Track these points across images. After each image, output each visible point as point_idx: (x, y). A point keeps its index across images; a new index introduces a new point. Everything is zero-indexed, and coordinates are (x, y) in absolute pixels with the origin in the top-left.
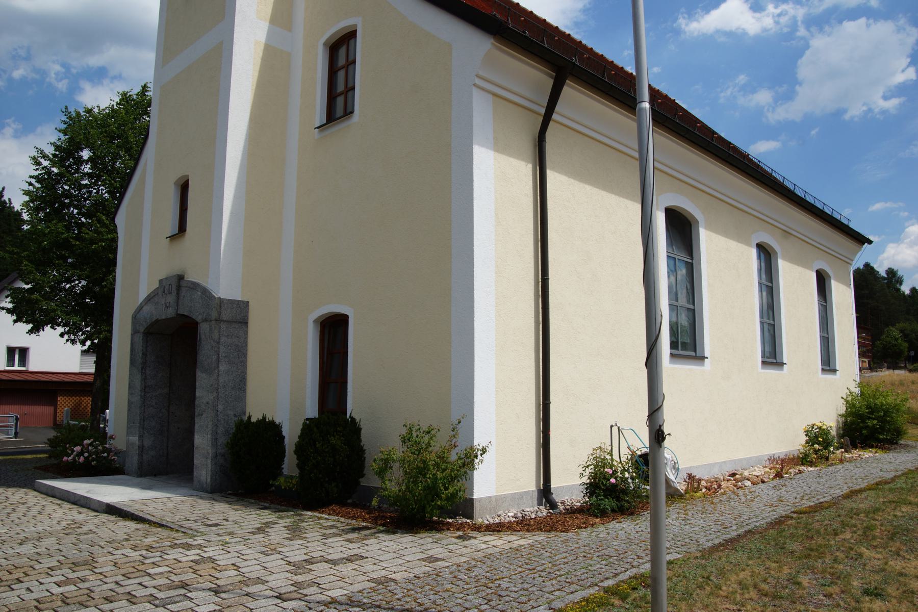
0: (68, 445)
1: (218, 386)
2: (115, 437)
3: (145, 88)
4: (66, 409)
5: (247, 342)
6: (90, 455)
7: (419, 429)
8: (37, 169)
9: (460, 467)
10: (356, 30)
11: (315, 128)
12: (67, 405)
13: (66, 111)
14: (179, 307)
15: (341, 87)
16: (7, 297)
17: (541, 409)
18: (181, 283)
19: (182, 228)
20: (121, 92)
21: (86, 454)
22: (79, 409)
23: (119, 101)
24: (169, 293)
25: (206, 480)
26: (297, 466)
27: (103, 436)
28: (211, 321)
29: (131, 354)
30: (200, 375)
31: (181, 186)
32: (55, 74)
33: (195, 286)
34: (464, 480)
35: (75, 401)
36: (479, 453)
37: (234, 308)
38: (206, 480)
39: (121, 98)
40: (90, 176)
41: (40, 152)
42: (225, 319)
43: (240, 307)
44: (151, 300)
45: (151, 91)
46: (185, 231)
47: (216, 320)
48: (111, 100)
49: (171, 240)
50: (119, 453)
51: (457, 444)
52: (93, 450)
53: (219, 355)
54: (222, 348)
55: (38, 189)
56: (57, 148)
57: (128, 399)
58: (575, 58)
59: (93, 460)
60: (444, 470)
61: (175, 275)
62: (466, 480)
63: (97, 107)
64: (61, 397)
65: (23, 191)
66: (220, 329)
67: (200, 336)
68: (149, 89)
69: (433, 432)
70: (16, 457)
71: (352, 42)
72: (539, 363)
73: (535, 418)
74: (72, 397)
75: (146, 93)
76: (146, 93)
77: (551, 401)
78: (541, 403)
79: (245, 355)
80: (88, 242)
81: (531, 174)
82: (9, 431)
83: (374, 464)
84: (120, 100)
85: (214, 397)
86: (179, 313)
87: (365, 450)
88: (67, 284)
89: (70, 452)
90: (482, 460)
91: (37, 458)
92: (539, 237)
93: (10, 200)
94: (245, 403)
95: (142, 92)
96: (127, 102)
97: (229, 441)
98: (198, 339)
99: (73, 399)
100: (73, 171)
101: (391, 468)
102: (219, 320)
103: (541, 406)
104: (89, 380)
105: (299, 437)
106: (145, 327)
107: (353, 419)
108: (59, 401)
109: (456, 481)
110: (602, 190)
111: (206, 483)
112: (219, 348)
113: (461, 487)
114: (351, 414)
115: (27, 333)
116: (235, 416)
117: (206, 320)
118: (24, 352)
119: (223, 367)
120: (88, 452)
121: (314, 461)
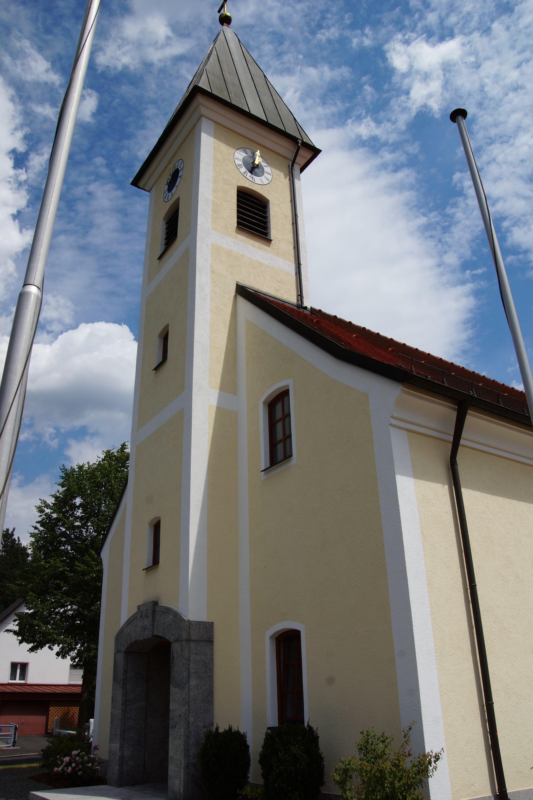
0: (58, 756)
1: (189, 699)
2: (99, 747)
3: (123, 446)
4: (56, 718)
5: (213, 658)
6: (77, 766)
7: (374, 736)
8: (41, 516)
9: (416, 774)
10: (289, 389)
11: (261, 471)
12: (57, 714)
13: (64, 470)
14: (154, 629)
15: (280, 436)
16: (15, 621)
17: (485, 710)
18: (155, 608)
19: (156, 560)
20: (105, 450)
21: (74, 765)
22: (67, 718)
23: (104, 458)
24: (146, 618)
25: (180, 790)
26: (262, 776)
27: (87, 747)
28: (182, 641)
29: (114, 671)
30: (173, 690)
31: (154, 525)
32: (49, 435)
33: (168, 611)
34: (420, 787)
35: (64, 711)
36: (433, 760)
37: (201, 628)
38: (180, 790)
39: (105, 455)
40: (81, 519)
41: (43, 502)
42: (194, 639)
43: (206, 628)
44: (131, 623)
45: (128, 448)
46: (158, 563)
47: (186, 640)
48: (98, 457)
49: (147, 572)
50: (102, 763)
51: (411, 752)
52: (80, 761)
53: (189, 671)
54: (192, 664)
55: (41, 532)
56: (56, 498)
57: (111, 712)
58: (472, 391)
59: (80, 770)
60: (401, 779)
61: (150, 602)
62: (422, 788)
63: (87, 463)
64: (52, 707)
65: (30, 533)
66: (190, 648)
67: (173, 655)
68: (127, 447)
69: (387, 741)
70: (14, 766)
71: (286, 399)
72: (478, 664)
73: (481, 719)
74: (61, 707)
75: (125, 450)
76: (125, 450)
77: (493, 701)
78: (485, 704)
79: (212, 670)
80: (80, 573)
81: (448, 493)
82: (9, 739)
83: (335, 774)
84: (105, 457)
85: (186, 710)
86: (154, 634)
87: (323, 758)
88: (61, 609)
89: (60, 763)
90: (436, 767)
91: (31, 767)
92: (463, 548)
93: (19, 538)
94: (213, 714)
95: (122, 449)
96: (110, 458)
97: (200, 751)
98: (171, 657)
99: (63, 709)
100: (68, 515)
101: (351, 777)
102: (189, 640)
103: (485, 707)
104: (76, 692)
105: (263, 747)
106: (126, 647)
107: (310, 728)
108: (51, 711)
109: (412, 789)
110: (513, 499)
111: (179, 793)
112: (189, 665)
113: (418, 796)
114: (308, 722)
115: (28, 651)
116: (204, 727)
117: (177, 640)
118: (24, 666)
119: (193, 682)
120: (75, 762)
121: (277, 770)
